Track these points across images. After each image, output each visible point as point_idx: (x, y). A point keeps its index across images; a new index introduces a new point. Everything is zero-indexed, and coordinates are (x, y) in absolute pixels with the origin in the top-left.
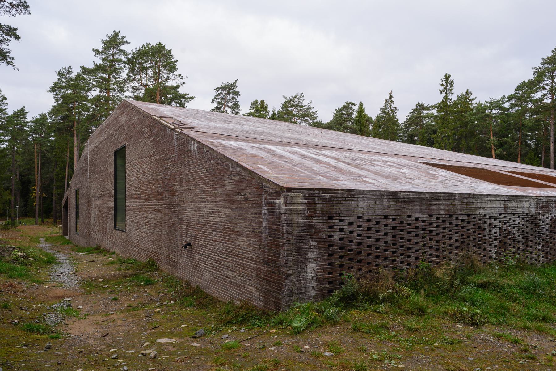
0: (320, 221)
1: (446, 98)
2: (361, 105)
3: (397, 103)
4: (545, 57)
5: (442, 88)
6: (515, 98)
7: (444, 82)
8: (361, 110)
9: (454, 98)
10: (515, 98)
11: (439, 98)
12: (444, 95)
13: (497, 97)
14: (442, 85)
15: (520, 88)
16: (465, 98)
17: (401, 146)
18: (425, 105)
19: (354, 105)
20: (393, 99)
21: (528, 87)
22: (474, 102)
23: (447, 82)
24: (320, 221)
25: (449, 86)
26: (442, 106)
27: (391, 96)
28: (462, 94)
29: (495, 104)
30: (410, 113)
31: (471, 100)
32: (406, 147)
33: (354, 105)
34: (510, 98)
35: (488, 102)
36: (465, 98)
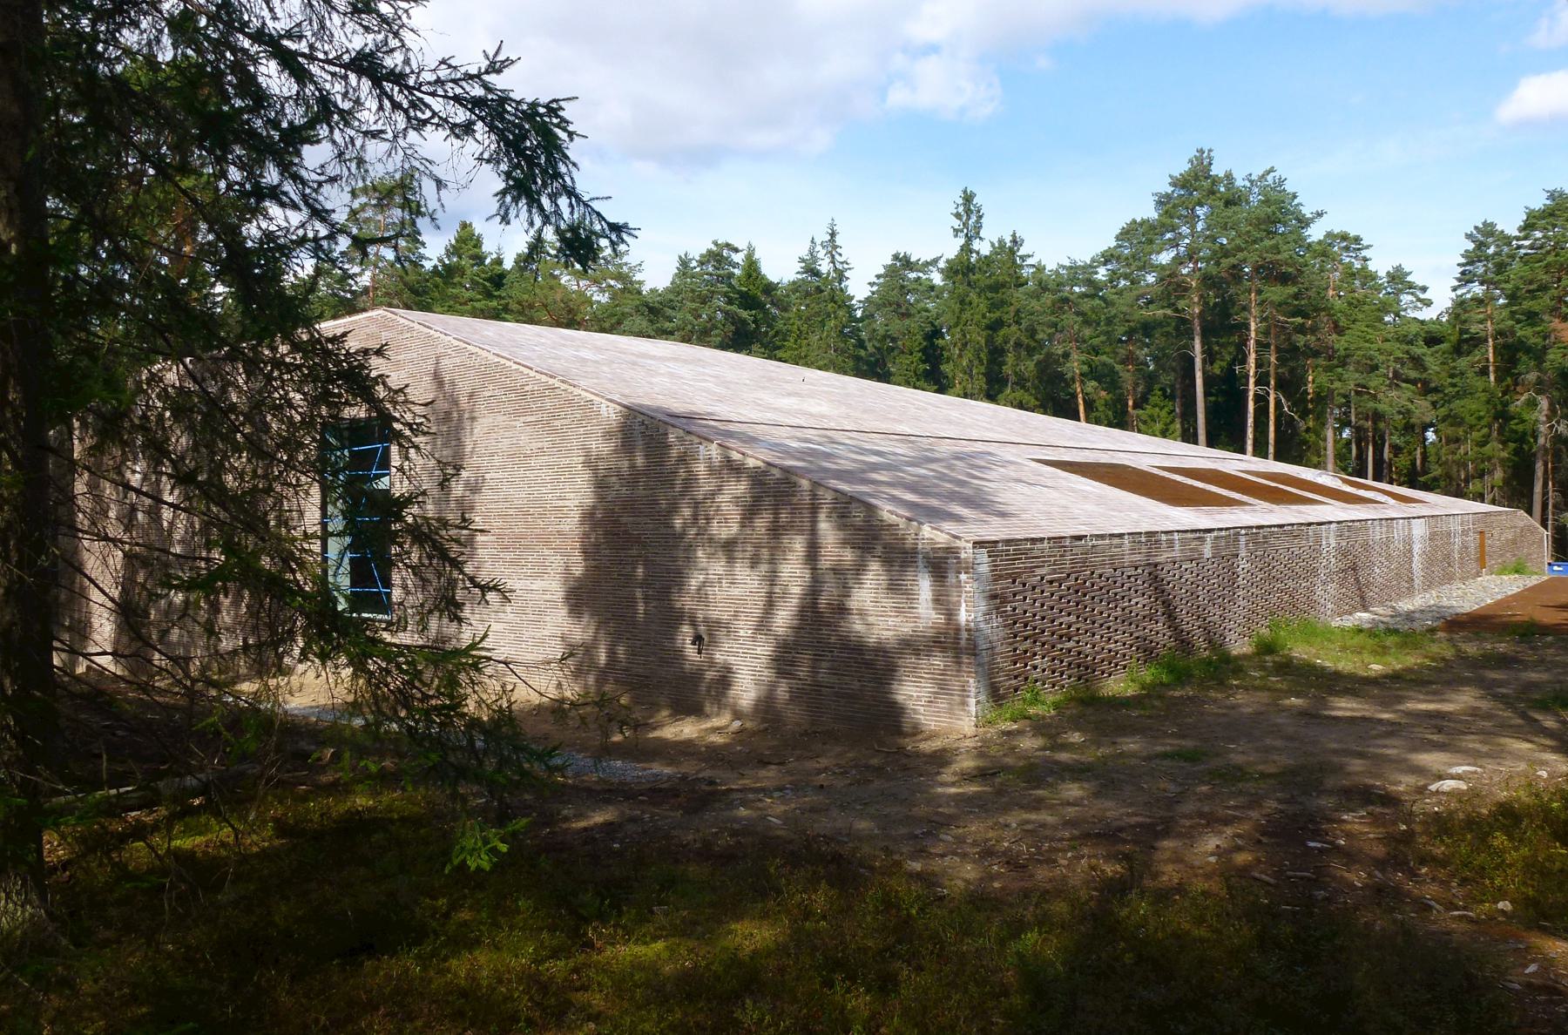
0: (900, 512)
1: (967, 249)
2: (751, 253)
3: (847, 252)
4: (1176, 174)
5: (957, 223)
6: (1118, 258)
7: (961, 209)
8: (752, 266)
9: (983, 248)
10: (1118, 258)
11: (950, 248)
12: (962, 241)
13: (1084, 256)
14: (958, 216)
15: (1126, 234)
16: (1009, 252)
17: (598, 349)
18: (913, 259)
19: (736, 250)
20: (838, 238)
21: (1139, 236)
22: (1029, 261)
23: (968, 212)
24: (900, 512)
25: (974, 219)
26: (961, 269)
27: (833, 235)
28: (1001, 241)
29: (1079, 273)
30: (878, 277)
31: (1022, 258)
32: (698, 361)
33: (736, 250)
34: (1107, 257)
35: (1064, 267)
36: (1009, 252)
